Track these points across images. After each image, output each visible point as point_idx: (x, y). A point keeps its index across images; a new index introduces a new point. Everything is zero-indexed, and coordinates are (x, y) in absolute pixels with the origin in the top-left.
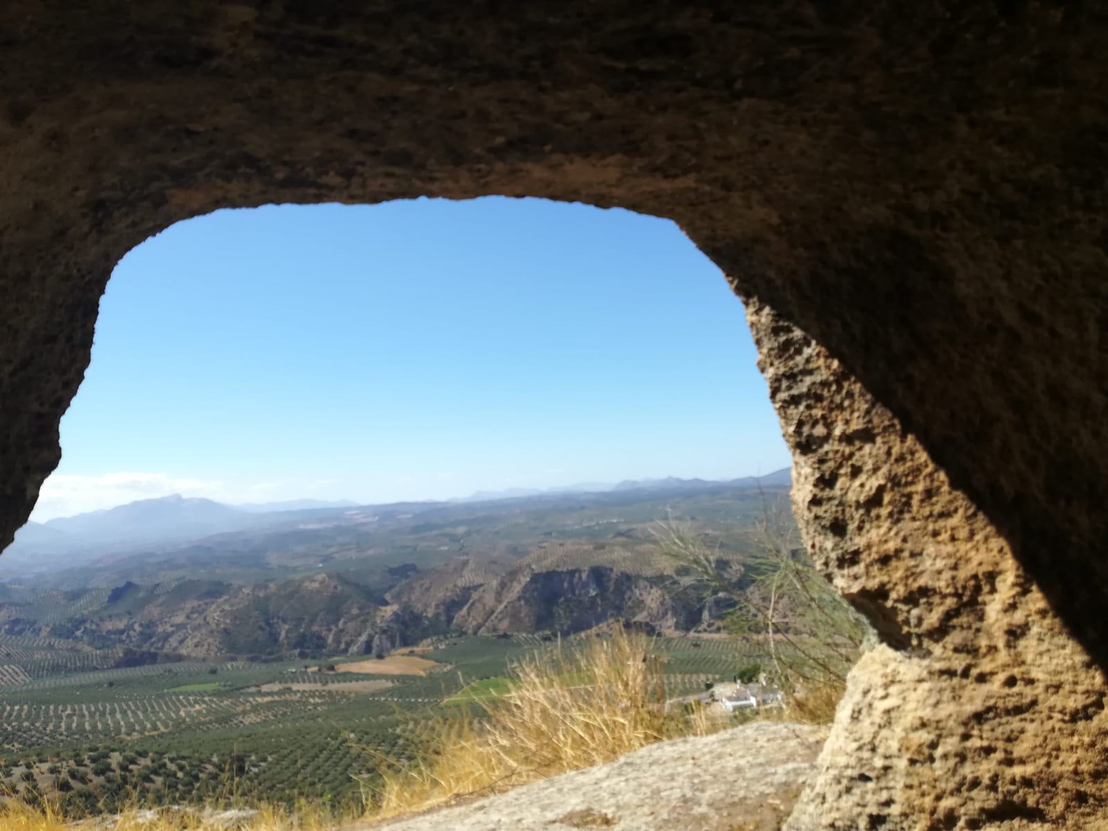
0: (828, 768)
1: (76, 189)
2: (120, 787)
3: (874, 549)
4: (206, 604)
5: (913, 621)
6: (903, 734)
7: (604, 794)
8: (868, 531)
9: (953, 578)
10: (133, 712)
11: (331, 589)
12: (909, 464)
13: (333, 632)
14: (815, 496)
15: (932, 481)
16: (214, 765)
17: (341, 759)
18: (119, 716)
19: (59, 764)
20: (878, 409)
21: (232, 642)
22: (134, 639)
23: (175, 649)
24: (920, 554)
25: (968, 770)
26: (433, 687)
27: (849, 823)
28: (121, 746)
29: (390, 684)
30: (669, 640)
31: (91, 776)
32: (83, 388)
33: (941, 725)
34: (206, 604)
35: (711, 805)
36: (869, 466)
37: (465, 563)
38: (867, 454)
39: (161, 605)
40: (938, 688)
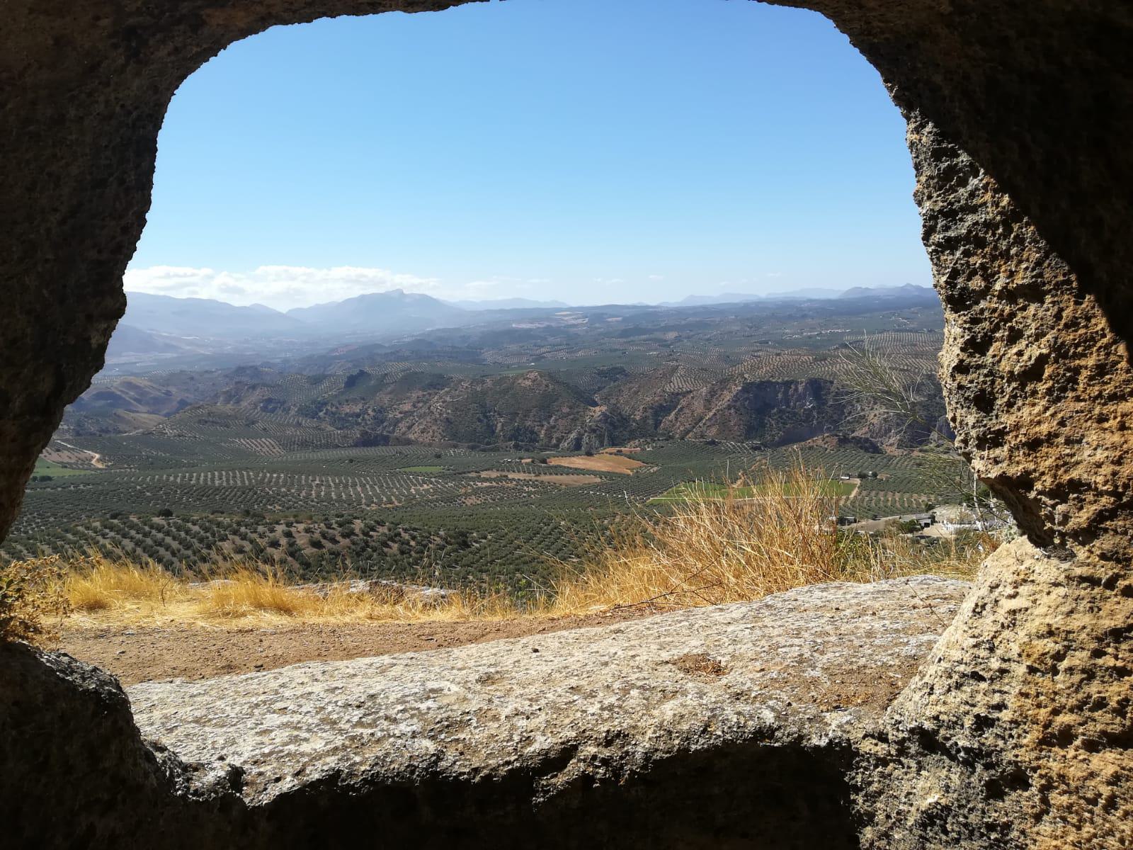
0: (940, 660)
1: (98, 18)
2: (363, 550)
3: (1023, 431)
4: (430, 394)
5: (1058, 518)
6: (1026, 639)
7: (726, 639)
8: (1019, 409)
9: (1114, 474)
10: (371, 486)
11: (543, 388)
12: (1082, 331)
13: (545, 428)
14: (961, 361)
15: (1108, 354)
16: (441, 537)
17: (553, 543)
18: (359, 489)
19: (312, 526)
20: (1053, 260)
21: (453, 431)
22: (368, 423)
23: (404, 434)
24: (1079, 442)
25: (1094, 689)
26: (642, 486)
27: (955, 719)
28: (362, 515)
29: (598, 480)
30: (891, 458)
31: (339, 538)
32: (146, 232)
33: (1071, 636)
34: (430, 394)
35: (825, 669)
36: (1031, 331)
37: (675, 369)
38: (1032, 315)
39: (390, 393)
40: (1075, 596)
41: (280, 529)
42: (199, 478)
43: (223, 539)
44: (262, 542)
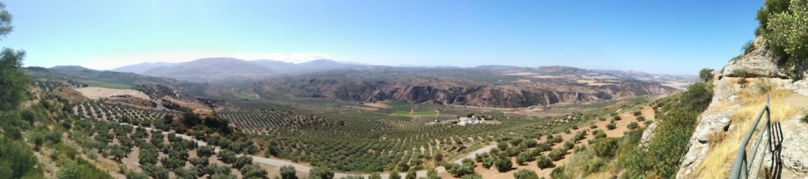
2: (316, 124)
31: (310, 120)
37: (397, 82)
41: (296, 116)
42: (278, 102)
43: (285, 118)
44: (293, 119)
